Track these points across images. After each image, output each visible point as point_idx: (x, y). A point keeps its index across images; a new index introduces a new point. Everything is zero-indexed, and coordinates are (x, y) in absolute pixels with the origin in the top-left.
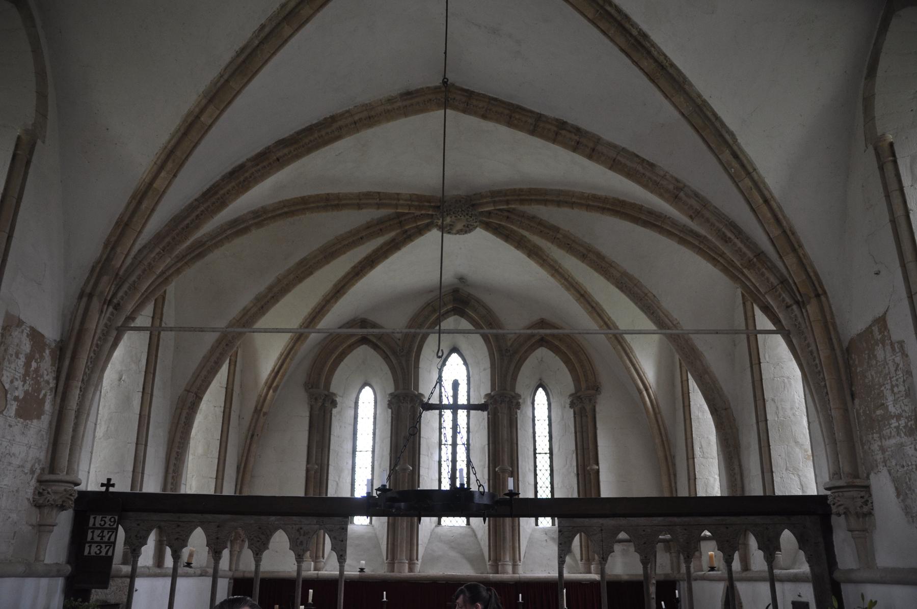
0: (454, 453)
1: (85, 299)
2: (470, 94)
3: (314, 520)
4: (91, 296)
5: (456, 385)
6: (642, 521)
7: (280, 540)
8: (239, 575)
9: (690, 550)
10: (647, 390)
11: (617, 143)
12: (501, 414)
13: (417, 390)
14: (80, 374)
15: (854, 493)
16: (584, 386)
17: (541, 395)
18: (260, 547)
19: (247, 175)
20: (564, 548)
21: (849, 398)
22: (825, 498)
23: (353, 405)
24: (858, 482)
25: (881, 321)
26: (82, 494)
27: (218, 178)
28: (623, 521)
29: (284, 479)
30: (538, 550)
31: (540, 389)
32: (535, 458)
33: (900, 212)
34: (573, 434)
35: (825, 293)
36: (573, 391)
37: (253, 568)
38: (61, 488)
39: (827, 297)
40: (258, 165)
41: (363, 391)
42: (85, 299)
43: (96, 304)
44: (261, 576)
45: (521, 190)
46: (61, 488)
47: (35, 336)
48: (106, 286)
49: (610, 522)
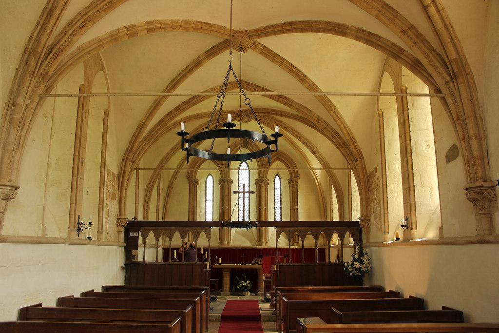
0: (244, 201)
1: (125, 161)
2: (248, 84)
3: (200, 228)
4: (126, 160)
5: (244, 185)
6: (303, 228)
7: (177, 235)
8: (165, 247)
9: (329, 237)
10: (316, 178)
11: (299, 103)
12: (261, 185)
13: (229, 177)
14: (125, 185)
15: (365, 221)
16: (293, 176)
17: (277, 179)
18: (196, 237)
19: (173, 115)
20: (278, 237)
21: (368, 191)
22: (358, 222)
23: (204, 183)
24: (367, 218)
25: (376, 169)
26: (128, 221)
27: (163, 116)
28: (296, 228)
29: (179, 214)
30: (272, 239)
31: (277, 176)
32: (275, 203)
33: (382, 137)
34: (289, 195)
35: (363, 158)
36: (289, 178)
37: (169, 245)
38: (123, 220)
39: (364, 160)
40: (176, 111)
41: (209, 177)
42: (125, 161)
43: (128, 162)
44: (172, 247)
45: (268, 109)
46: (123, 220)
47: (113, 174)
48: (131, 156)
49: (292, 229)
